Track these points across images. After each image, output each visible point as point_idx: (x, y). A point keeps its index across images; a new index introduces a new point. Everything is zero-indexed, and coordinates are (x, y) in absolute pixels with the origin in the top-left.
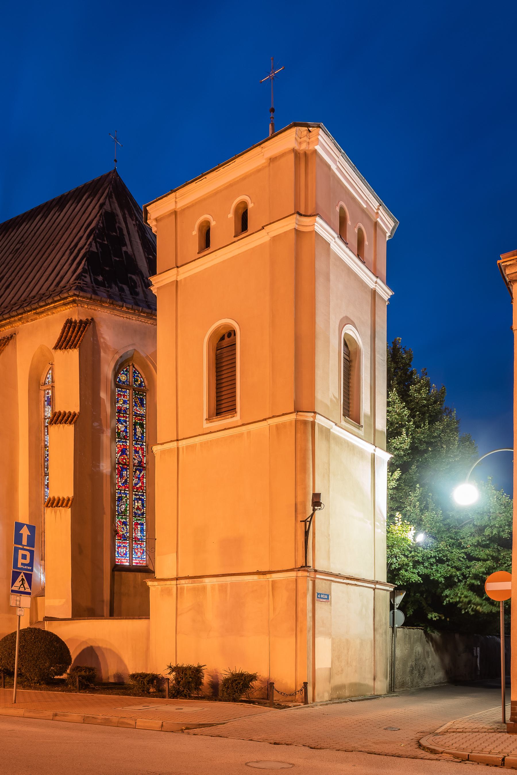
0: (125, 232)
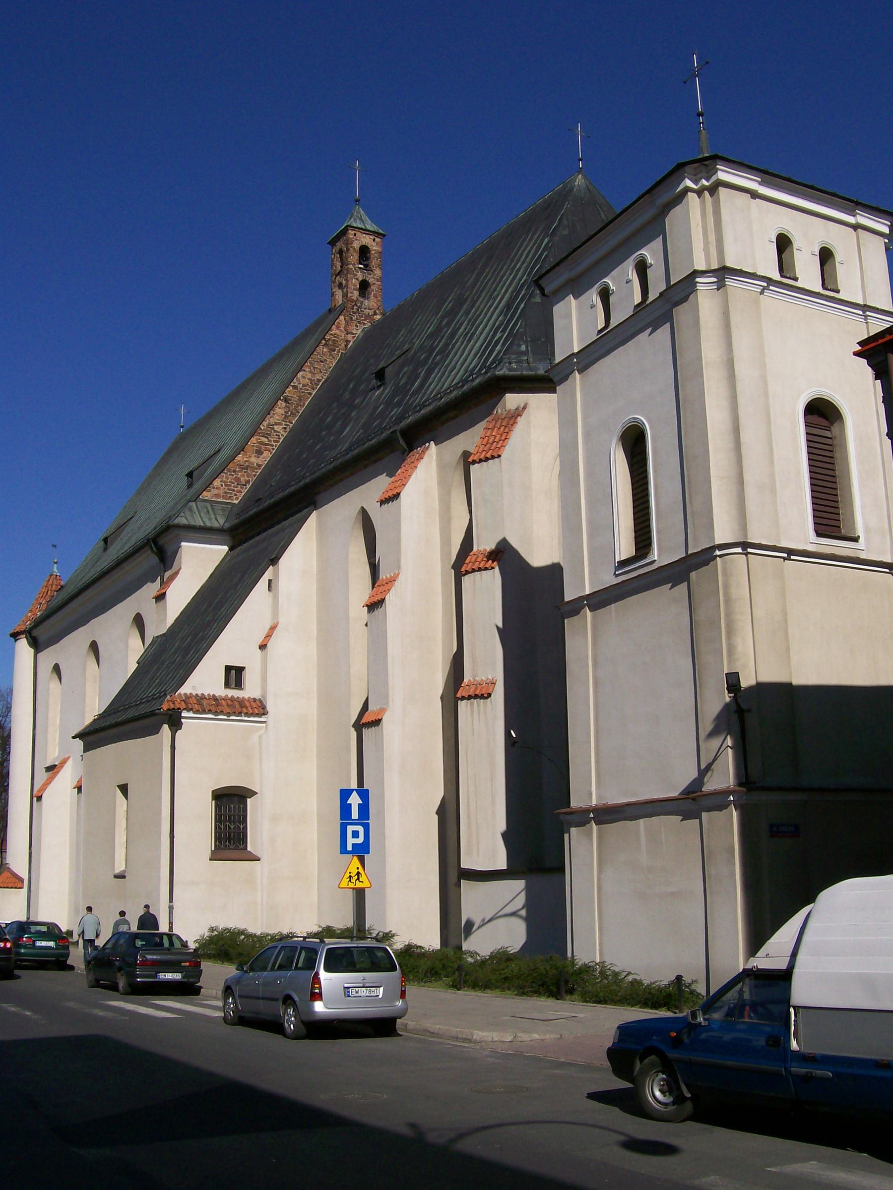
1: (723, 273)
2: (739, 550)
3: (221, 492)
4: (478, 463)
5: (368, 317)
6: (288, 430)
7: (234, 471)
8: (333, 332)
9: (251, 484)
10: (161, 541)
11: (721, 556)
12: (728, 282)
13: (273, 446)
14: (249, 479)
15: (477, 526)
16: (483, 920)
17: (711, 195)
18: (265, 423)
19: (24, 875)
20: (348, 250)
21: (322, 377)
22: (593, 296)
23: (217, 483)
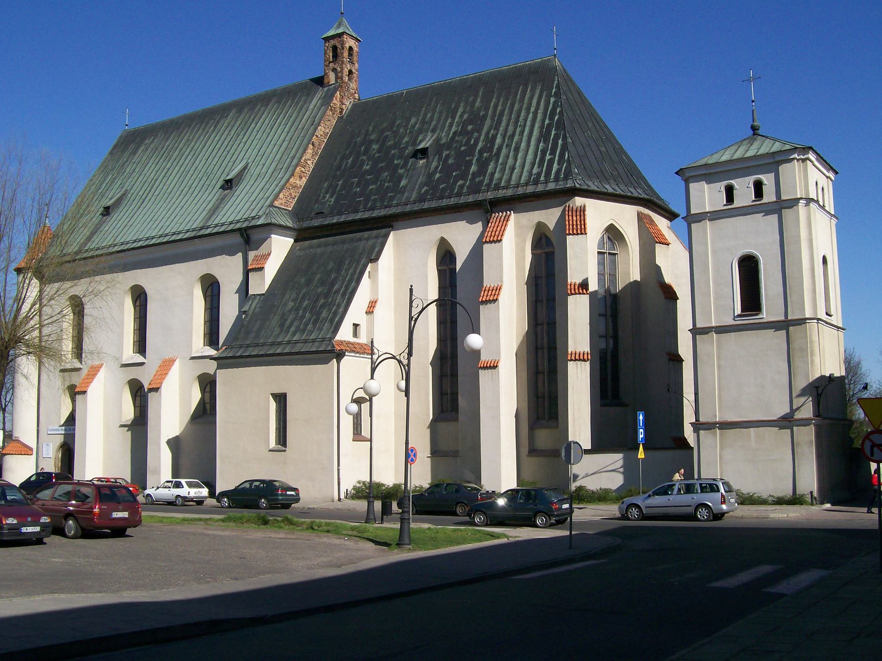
0: (362, 356)
1: (809, 200)
2: (816, 321)
3: (283, 202)
4: (572, 235)
5: (352, 94)
6: (314, 164)
7: (289, 189)
8: (334, 102)
9: (297, 198)
10: (250, 232)
11: (808, 323)
12: (811, 204)
13: (306, 174)
14: (296, 194)
15: (571, 269)
16: (587, 474)
17: (797, 162)
18: (303, 158)
19: (33, 445)
20: (343, 48)
21: (329, 131)
22: (722, 186)
23: (281, 196)
